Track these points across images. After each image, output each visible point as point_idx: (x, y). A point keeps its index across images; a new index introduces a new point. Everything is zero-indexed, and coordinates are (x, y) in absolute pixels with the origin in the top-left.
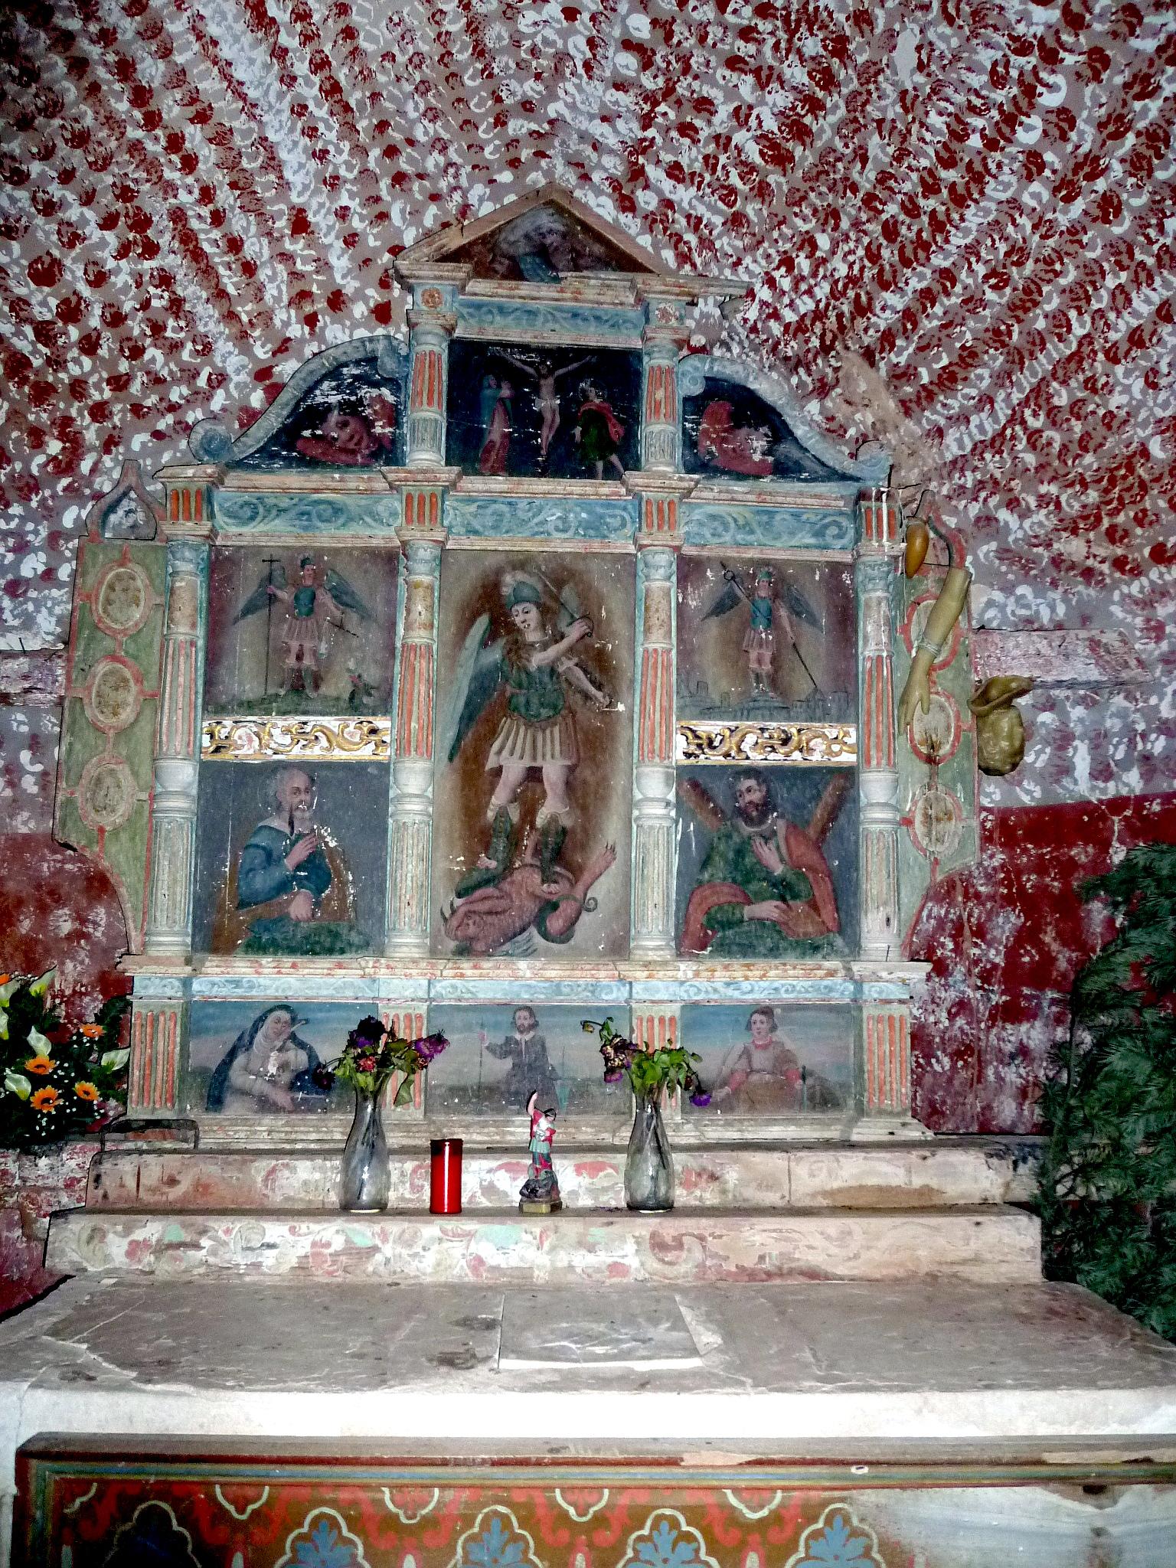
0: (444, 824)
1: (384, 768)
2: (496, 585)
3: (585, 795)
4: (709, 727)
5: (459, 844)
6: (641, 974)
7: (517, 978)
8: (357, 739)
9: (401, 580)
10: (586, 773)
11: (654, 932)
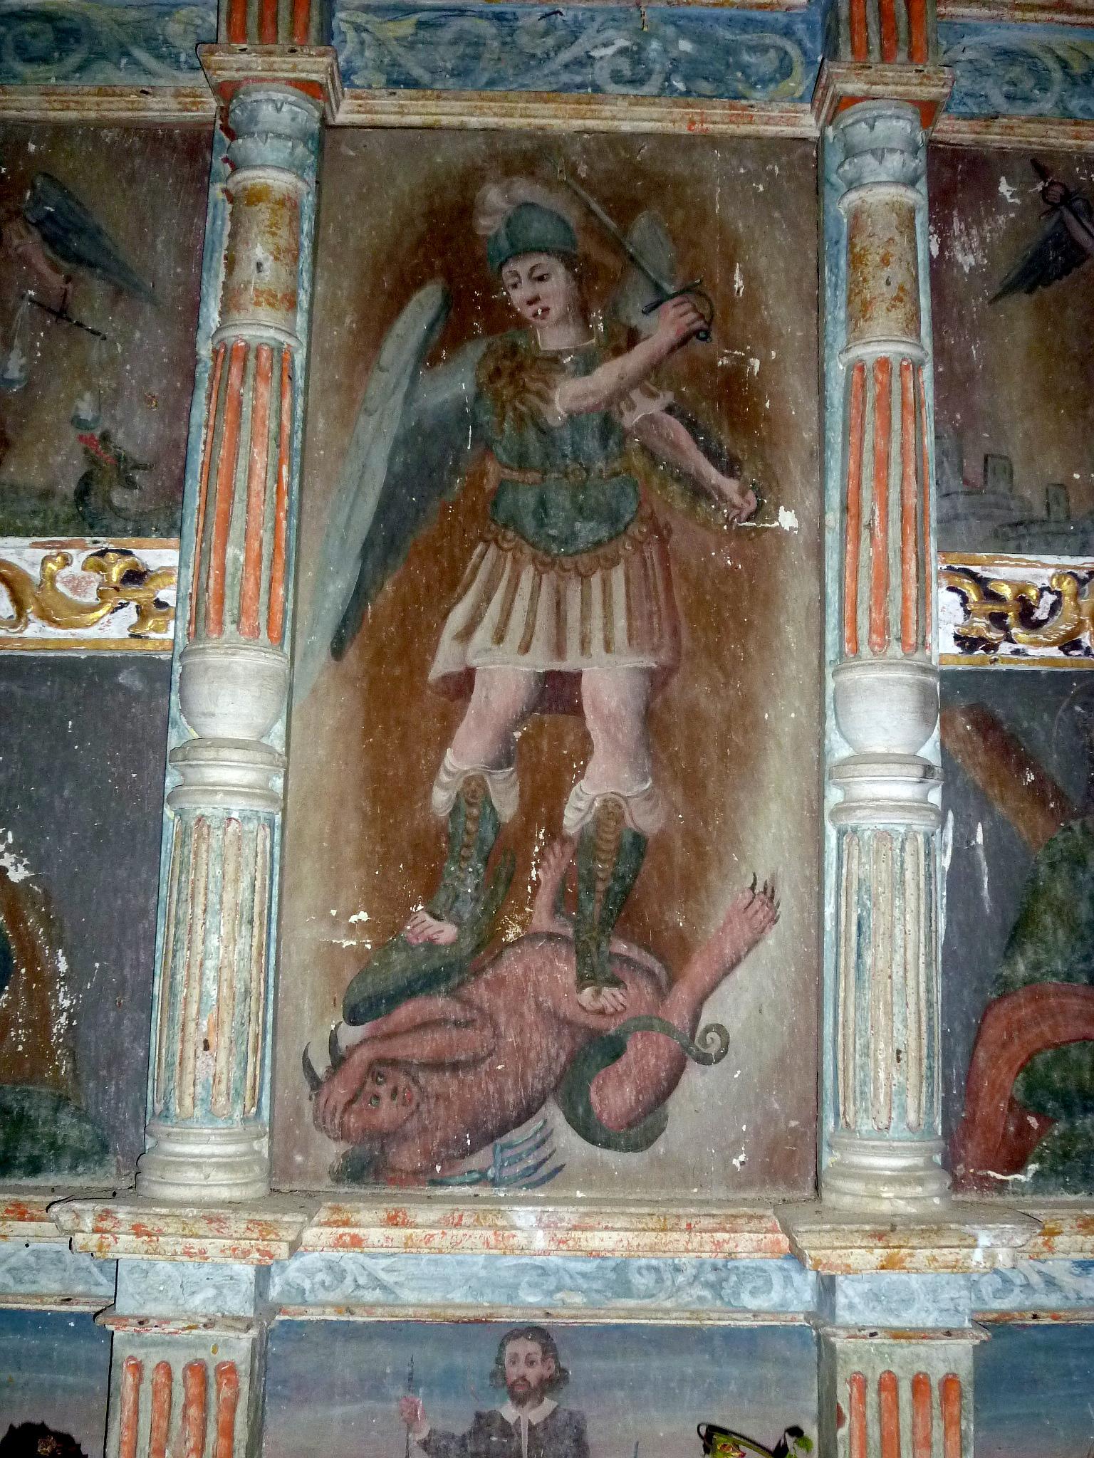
0: (317, 823)
1: (158, 673)
2: (465, 211)
3: (694, 745)
4: (1011, 572)
5: (356, 876)
6: (865, 1257)
7: (508, 1251)
8: (91, 598)
9: (216, 191)
10: (697, 691)
11: (886, 1136)
